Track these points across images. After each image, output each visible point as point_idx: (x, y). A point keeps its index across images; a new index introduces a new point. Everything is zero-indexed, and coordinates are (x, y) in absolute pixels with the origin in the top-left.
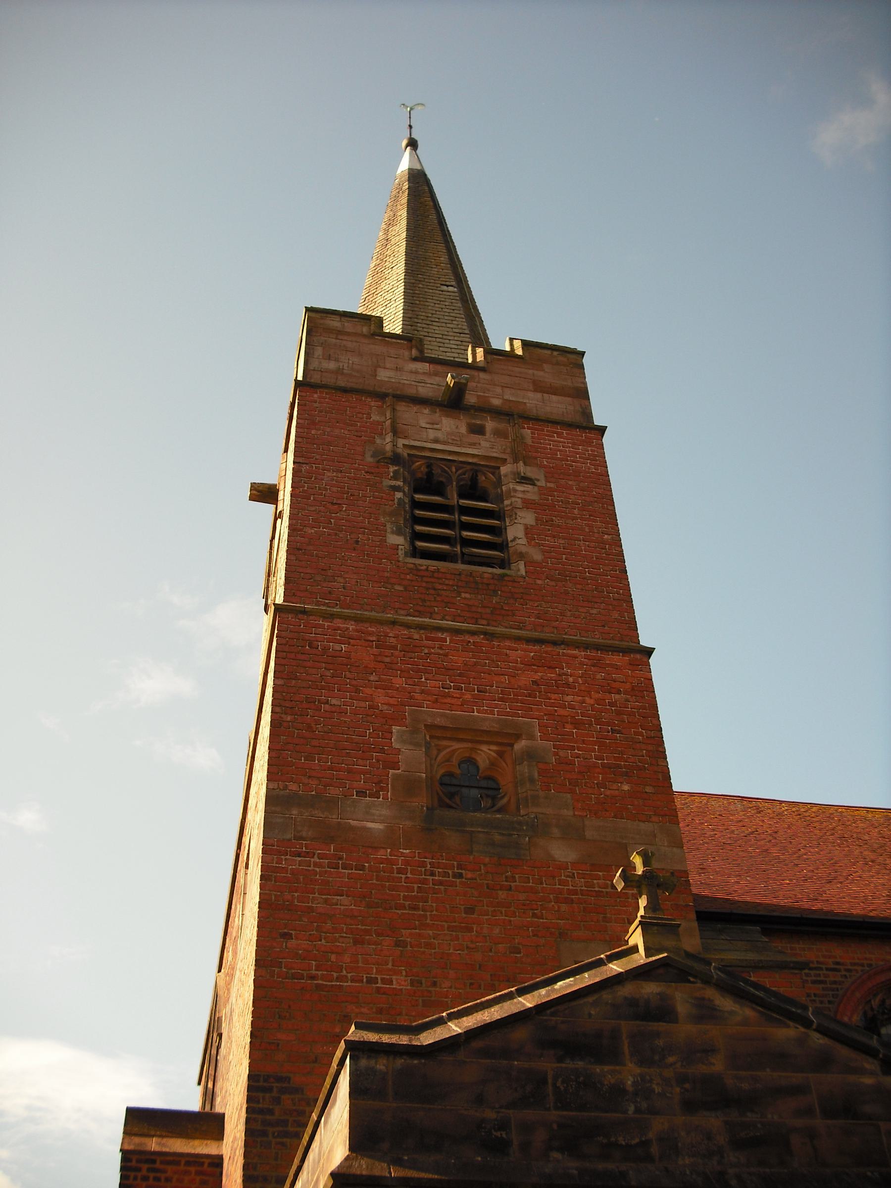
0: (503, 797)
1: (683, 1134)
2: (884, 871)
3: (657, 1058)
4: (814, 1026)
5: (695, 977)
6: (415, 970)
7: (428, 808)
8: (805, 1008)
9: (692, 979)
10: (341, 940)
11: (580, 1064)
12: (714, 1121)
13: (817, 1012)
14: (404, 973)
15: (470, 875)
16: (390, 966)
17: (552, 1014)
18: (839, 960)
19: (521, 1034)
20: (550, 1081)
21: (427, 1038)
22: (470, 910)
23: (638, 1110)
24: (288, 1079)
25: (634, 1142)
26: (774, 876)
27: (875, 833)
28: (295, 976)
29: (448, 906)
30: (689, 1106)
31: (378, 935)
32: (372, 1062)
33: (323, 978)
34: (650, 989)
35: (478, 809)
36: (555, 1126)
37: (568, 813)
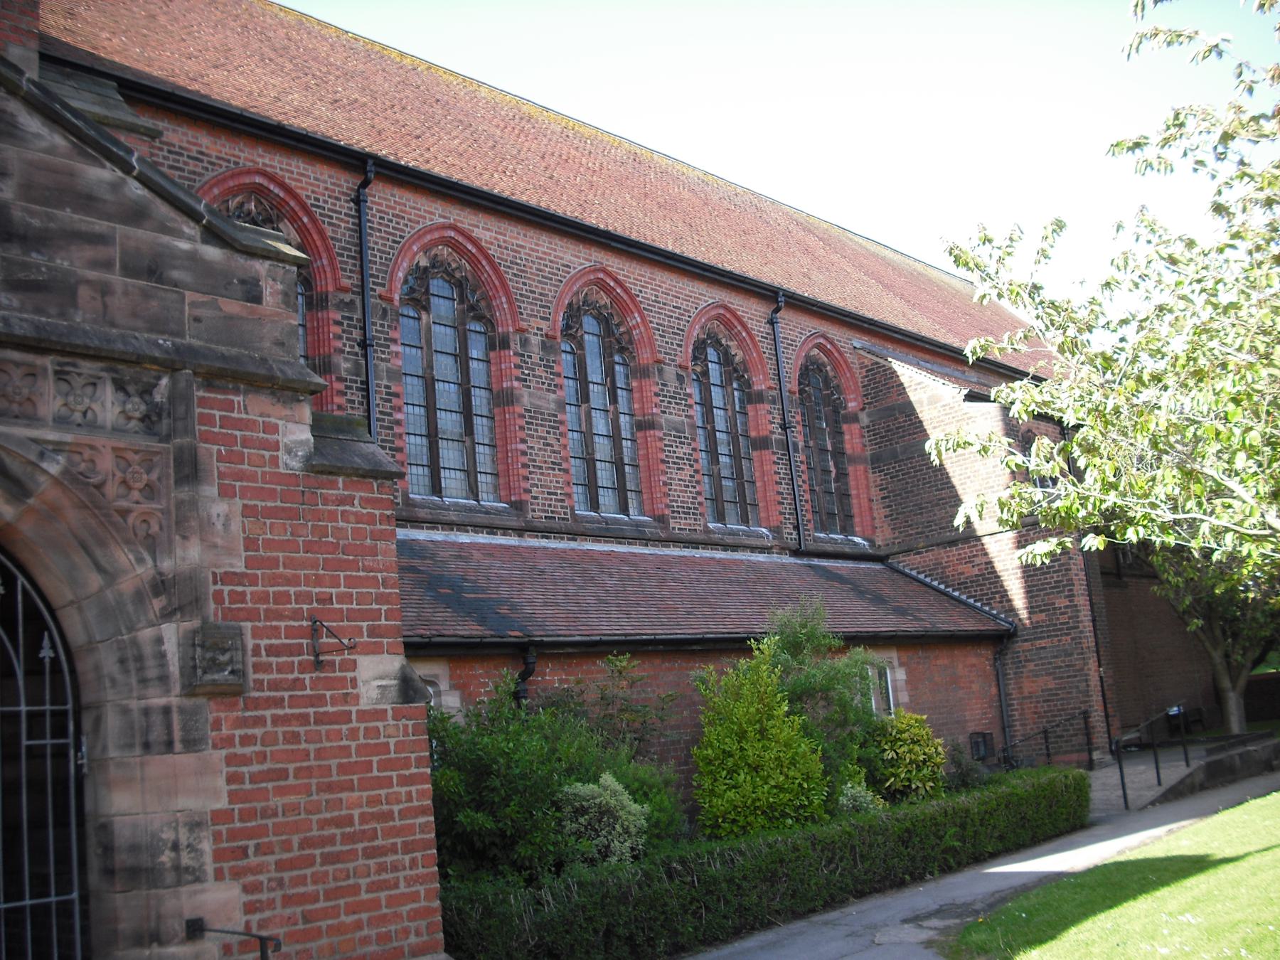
2: (279, 73)
4: (135, 173)
13: (140, 160)
18: (204, 150)
26: (153, 44)
27: (282, 32)
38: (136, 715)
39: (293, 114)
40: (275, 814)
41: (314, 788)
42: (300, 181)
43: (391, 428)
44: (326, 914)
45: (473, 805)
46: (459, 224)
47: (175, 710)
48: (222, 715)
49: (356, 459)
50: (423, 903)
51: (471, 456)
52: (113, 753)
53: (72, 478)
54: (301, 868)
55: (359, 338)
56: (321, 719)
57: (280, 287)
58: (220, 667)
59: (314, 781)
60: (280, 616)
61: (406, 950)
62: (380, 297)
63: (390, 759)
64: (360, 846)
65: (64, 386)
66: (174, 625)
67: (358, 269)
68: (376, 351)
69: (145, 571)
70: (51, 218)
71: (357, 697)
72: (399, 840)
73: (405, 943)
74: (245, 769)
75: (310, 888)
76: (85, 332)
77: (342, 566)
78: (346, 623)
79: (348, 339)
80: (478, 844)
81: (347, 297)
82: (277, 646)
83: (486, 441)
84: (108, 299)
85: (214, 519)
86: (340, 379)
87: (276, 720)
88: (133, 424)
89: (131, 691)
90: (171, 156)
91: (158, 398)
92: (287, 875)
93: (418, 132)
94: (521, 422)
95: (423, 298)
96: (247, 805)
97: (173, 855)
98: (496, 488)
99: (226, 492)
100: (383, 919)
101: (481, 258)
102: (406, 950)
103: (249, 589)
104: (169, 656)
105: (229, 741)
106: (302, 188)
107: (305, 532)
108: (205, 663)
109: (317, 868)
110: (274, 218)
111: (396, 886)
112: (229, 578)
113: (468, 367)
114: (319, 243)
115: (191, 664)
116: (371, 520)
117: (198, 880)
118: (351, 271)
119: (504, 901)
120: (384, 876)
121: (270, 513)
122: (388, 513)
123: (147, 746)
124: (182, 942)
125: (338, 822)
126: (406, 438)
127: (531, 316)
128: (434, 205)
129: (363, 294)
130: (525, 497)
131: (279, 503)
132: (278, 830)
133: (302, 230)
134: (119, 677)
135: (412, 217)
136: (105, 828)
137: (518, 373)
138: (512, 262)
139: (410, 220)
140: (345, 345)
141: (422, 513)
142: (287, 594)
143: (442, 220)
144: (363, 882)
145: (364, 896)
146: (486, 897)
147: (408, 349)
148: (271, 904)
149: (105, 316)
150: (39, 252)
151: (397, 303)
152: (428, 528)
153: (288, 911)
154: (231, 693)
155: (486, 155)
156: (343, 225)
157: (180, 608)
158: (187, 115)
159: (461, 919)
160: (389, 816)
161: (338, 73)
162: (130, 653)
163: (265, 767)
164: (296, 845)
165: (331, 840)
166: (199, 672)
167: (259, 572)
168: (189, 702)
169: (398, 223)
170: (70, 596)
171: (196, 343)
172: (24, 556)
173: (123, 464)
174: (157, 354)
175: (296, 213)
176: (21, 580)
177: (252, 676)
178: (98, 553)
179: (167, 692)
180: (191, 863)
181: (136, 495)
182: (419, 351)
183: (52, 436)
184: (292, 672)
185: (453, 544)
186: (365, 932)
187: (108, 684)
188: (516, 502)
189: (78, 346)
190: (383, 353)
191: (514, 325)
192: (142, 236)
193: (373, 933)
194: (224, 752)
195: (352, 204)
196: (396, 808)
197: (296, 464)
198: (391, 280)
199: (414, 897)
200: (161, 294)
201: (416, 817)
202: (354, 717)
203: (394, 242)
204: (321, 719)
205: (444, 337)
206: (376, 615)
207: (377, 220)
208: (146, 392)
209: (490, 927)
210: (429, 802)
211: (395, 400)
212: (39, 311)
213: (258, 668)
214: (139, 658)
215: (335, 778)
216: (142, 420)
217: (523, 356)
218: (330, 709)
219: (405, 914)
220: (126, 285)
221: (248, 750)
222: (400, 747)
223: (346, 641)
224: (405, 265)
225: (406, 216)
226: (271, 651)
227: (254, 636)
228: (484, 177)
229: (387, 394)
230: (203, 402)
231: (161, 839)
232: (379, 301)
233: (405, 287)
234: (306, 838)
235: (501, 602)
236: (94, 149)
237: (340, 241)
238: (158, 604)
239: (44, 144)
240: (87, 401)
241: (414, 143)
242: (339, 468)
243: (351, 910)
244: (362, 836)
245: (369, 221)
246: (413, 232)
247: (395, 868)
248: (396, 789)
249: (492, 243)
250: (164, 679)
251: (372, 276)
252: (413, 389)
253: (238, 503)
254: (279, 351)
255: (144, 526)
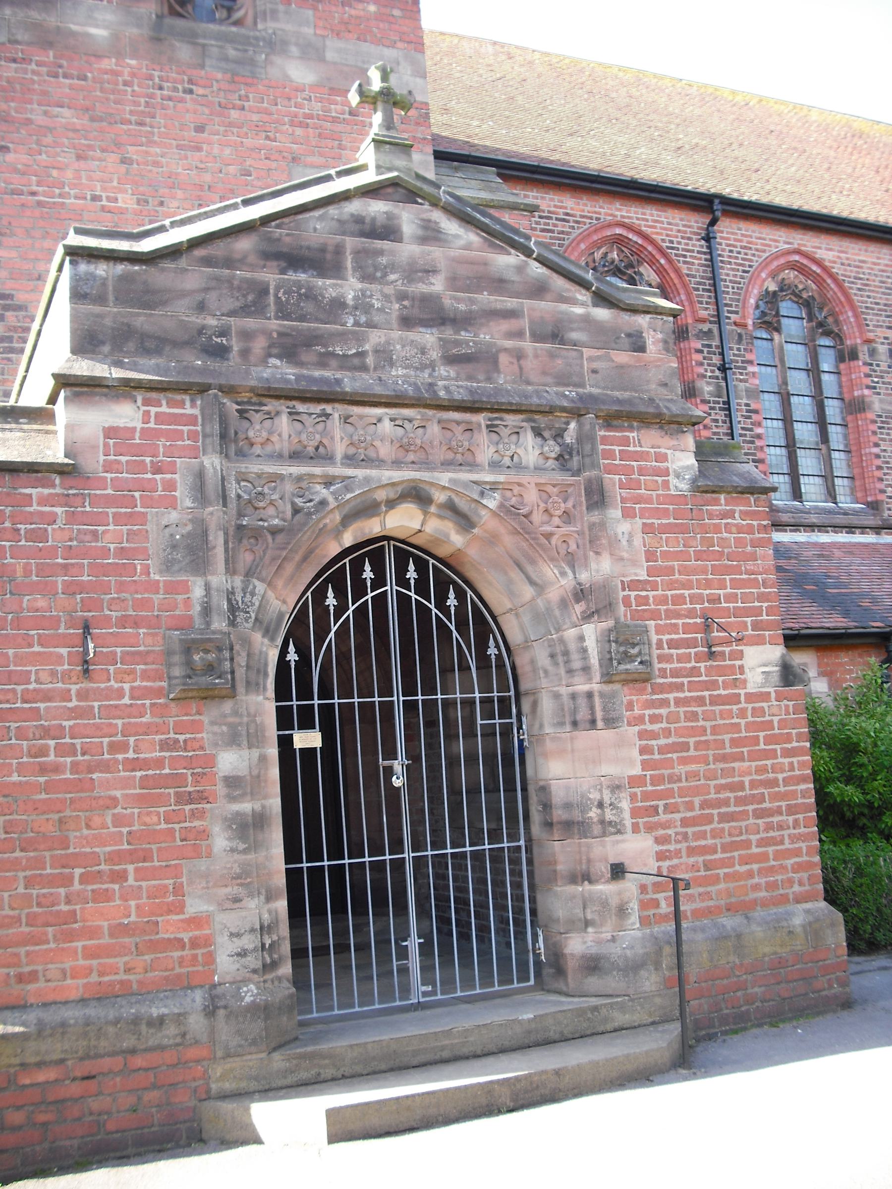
0: (239, 9)
1: (398, 347)
3: (379, 274)
5: (423, 198)
6: (141, 189)
7: (157, 16)
8: (528, 238)
9: (420, 201)
10: (63, 154)
11: (302, 276)
12: (428, 337)
14: (130, 191)
15: (201, 91)
16: (115, 184)
17: (278, 227)
19: (244, 244)
20: (272, 291)
21: (147, 245)
22: (200, 129)
23: (357, 324)
24: (10, 297)
25: (350, 353)
28: (14, 192)
29: (177, 123)
30: (407, 322)
31: (103, 150)
32: (92, 268)
33: (45, 194)
34: (377, 208)
35: (212, 20)
36: (275, 335)
37: (308, 31)
38: (566, 700)
39: (642, 167)
40: (680, 780)
41: (711, 758)
42: (655, 227)
43: (752, 442)
44: (723, 863)
45: (842, 779)
46: (803, 248)
47: (596, 694)
48: (634, 698)
49: (735, 478)
50: (805, 858)
51: (828, 462)
52: (548, 730)
53: (508, 511)
54: (702, 825)
55: (718, 363)
56: (714, 701)
57: (660, 336)
58: (631, 659)
59: (711, 752)
60: (678, 615)
61: (791, 897)
62: (735, 324)
63: (774, 735)
64: (750, 808)
65: (494, 435)
66: (593, 626)
67: (713, 300)
68: (734, 374)
69: (567, 582)
70: (472, 301)
71: (745, 682)
72: (783, 804)
73: (790, 891)
74: (654, 742)
75: (710, 842)
76: (507, 391)
77: (728, 570)
78: (733, 619)
79: (709, 365)
80: (848, 814)
81: (705, 327)
82: (677, 640)
83: (841, 448)
84: (521, 362)
85: (620, 536)
86: (704, 402)
87: (678, 702)
88: (551, 463)
89: (560, 679)
90: (542, 221)
91: (568, 440)
92: (690, 830)
93: (756, 166)
94: (873, 427)
95: (775, 319)
96: (657, 772)
97: (599, 811)
98: (853, 490)
99: (628, 514)
100: (771, 870)
101: (825, 276)
102: (791, 897)
103: (651, 594)
104: (590, 651)
105: (640, 720)
106: (657, 233)
107: (694, 544)
108: (619, 656)
109: (715, 825)
110: (635, 263)
111: (782, 842)
112: (634, 585)
113: (820, 380)
114: (676, 281)
115: (608, 656)
116: (750, 530)
117: (619, 832)
118: (707, 303)
119: (874, 863)
120: (772, 834)
121: (664, 529)
122: (765, 523)
123: (575, 724)
124: (607, 882)
125: (732, 787)
126: (766, 449)
127: (877, 326)
128: (778, 233)
129: (719, 323)
130: (881, 497)
131: (672, 520)
132: (682, 793)
133: (660, 271)
134: (550, 668)
135: (759, 247)
136: (544, 789)
137: (868, 381)
138: (856, 278)
139: (757, 250)
140: (706, 371)
141: (785, 518)
142: (683, 596)
143: (787, 246)
144: (754, 838)
145: (755, 850)
146: (858, 858)
147: (763, 368)
148: (678, 853)
149: (522, 377)
150: (466, 330)
151: (750, 328)
152: (791, 531)
153: (692, 860)
154: (641, 680)
155: (822, 177)
156: (696, 262)
157: (597, 611)
158: (552, 183)
159: (836, 877)
160: (774, 783)
161: (678, 121)
162: (558, 649)
163: (670, 741)
164: (697, 806)
165: (726, 802)
166: (615, 663)
167: (658, 579)
168: (607, 688)
169: (746, 254)
170: (509, 606)
171: (595, 391)
172: (471, 575)
173: (544, 495)
174: (565, 404)
175: (653, 256)
176: (470, 593)
177: (657, 666)
178: (529, 569)
179: (590, 680)
180: (613, 818)
181: (556, 521)
182: (774, 369)
183: (489, 478)
184: (690, 662)
185: (815, 544)
186: (756, 880)
187: (542, 675)
188: (872, 503)
189: (502, 404)
190: (741, 374)
191: (861, 337)
192: (544, 307)
193: (763, 881)
194: (637, 728)
195: (703, 242)
196: (780, 776)
197: (684, 486)
198: (744, 307)
199: (797, 853)
200: (564, 353)
201: (798, 784)
202: (742, 698)
203: (744, 271)
204: (714, 701)
205: (796, 355)
206: (758, 612)
207: (726, 254)
208: (559, 435)
209: (861, 885)
210: (809, 772)
211: (754, 416)
212: (470, 378)
213: (661, 658)
214: (566, 653)
215: (728, 750)
216: (557, 459)
217: (871, 365)
218: (722, 692)
219: (789, 867)
220: (535, 349)
221: (656, 727)
222: (783, 724)
223: (734, 634)
224: (756, 291)
225: (753, 246)
226: (672, 644)
227: (657, 633)
228: (823, 200)
229: (748, 411)
230: (604, 440)
231: (590, 799)
232: (734, 327)
233: (757, 312)
234: (705, 800)
235: (862, 596)
236: (501, 240)
237: (694, 277)
238: (579, 608)
239: (462, 242)
240: (513, 447)
241: (754, 176)
242: (722, 487)
243: (744, 861)
244: (752, 799)
245: (720, 255)
246: (760, 260)
247: (781, 827)
248: (780, 760)
249: (835, 262)
250: (586, 669)
251: (726, 305)
252: (770, 404)
253: (639, 522)
254: (663, 391)
255: (564, 545)
